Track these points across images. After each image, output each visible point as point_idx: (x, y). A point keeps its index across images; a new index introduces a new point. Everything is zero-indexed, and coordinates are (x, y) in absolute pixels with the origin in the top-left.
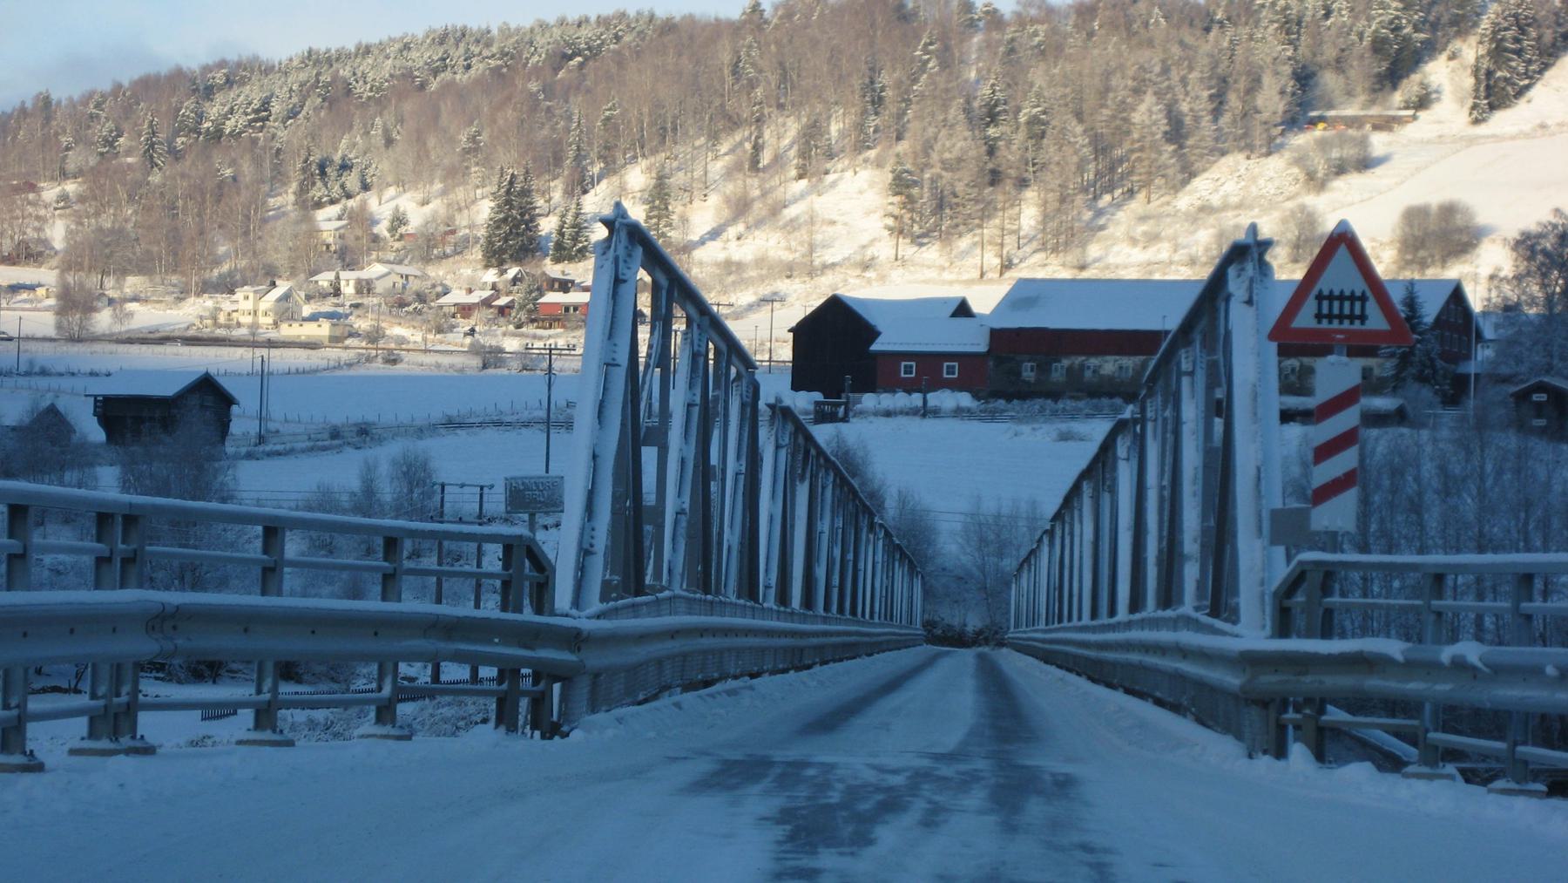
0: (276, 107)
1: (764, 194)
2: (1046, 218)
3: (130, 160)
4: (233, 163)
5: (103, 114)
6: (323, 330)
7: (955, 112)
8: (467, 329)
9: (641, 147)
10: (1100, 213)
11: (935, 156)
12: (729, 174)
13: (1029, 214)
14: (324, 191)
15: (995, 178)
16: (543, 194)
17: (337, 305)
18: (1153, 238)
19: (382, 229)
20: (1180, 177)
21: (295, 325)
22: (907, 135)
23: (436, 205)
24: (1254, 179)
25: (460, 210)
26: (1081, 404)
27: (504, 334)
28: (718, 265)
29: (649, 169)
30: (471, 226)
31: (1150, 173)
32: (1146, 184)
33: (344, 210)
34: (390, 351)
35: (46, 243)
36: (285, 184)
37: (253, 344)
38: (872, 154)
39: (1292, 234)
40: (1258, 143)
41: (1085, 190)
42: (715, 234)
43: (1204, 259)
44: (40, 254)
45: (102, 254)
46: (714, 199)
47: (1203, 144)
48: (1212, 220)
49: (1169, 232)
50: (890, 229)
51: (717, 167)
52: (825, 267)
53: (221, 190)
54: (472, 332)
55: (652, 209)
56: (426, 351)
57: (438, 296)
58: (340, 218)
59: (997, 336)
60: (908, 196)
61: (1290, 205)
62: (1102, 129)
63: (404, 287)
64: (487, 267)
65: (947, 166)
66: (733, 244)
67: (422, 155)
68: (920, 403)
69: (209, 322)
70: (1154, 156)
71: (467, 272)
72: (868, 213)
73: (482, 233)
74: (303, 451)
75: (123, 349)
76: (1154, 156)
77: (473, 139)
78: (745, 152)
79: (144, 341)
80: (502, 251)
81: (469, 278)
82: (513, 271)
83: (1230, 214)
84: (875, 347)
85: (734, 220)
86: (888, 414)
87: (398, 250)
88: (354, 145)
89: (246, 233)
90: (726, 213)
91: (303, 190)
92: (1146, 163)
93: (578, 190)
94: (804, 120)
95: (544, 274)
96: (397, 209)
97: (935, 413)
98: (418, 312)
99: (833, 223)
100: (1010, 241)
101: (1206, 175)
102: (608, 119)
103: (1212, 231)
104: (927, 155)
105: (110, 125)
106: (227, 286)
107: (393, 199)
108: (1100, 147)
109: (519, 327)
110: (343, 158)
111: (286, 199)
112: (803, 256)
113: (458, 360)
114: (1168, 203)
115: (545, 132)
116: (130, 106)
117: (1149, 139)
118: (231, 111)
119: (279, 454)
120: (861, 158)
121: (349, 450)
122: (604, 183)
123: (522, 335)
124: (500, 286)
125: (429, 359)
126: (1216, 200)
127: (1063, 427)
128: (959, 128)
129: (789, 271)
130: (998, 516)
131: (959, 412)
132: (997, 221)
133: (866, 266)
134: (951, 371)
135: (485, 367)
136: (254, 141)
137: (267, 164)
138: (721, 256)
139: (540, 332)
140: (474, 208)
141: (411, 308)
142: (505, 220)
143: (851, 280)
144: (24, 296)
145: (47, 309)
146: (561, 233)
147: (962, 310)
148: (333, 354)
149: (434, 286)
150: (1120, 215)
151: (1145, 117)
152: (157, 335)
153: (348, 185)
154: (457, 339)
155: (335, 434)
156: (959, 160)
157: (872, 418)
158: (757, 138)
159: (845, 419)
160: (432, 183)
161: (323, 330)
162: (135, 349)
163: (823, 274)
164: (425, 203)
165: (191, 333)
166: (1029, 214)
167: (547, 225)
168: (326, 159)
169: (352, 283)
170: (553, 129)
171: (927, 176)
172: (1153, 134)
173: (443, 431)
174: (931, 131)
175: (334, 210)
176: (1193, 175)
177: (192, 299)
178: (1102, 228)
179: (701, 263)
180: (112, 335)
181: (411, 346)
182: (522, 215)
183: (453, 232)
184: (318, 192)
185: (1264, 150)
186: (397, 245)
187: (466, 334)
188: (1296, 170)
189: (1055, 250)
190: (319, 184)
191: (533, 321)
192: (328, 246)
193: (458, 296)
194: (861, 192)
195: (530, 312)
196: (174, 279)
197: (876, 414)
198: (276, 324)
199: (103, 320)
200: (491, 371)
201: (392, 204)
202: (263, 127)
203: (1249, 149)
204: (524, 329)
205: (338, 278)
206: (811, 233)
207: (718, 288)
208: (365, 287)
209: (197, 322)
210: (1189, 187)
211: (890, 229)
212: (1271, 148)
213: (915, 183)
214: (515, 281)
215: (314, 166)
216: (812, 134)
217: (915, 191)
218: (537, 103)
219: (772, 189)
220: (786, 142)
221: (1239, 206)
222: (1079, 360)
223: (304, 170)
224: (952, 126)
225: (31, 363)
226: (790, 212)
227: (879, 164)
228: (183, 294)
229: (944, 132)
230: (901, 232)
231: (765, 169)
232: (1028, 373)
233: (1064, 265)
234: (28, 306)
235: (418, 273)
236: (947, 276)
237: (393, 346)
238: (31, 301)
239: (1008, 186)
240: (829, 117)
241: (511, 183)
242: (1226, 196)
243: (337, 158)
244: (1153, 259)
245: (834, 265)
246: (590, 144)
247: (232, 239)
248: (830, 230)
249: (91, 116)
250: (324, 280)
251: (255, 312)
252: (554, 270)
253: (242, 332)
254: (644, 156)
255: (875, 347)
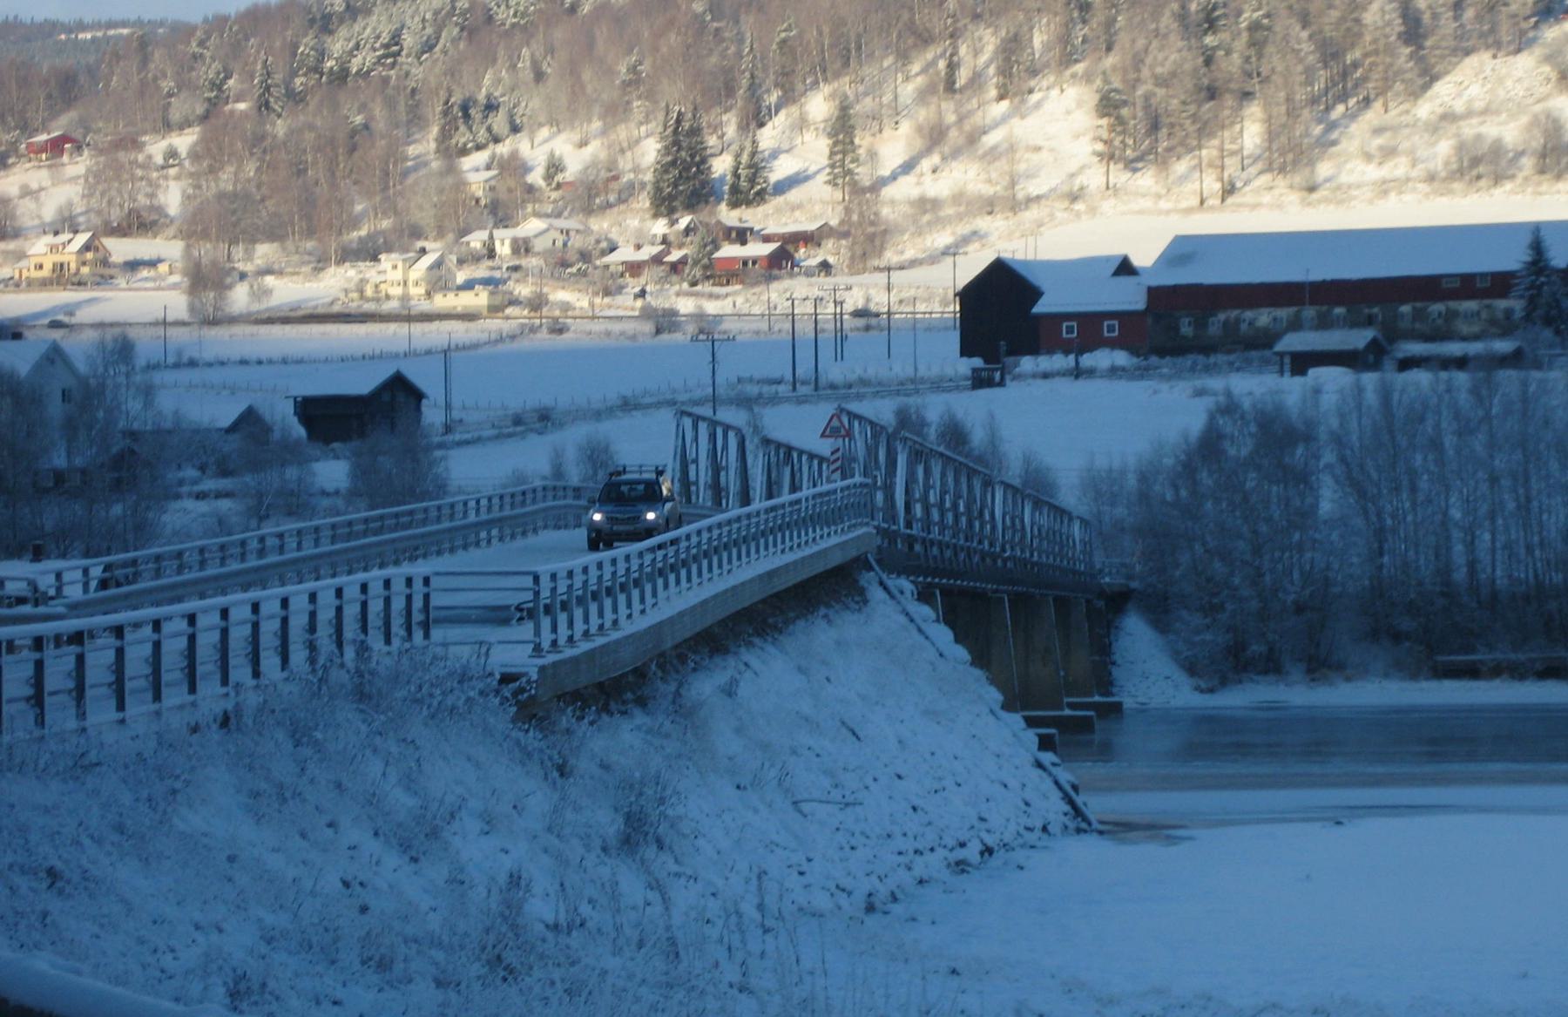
0: (408, 40)
1: (961, 120)
2: (1271, 136)
3: (242, 106)
4: (363, 108)
5: (207, 54)
6: (478, 299)
7: (1167, 21)
8: (637, 290)
9: (822, 73)
10: (1332, 126)
11: (1145, 73)
12: (923, 96)
13: (1251, 132)
14: (468, 136)
15: (1212, 93)
16: (715, 131)
17: (493, 268)
18: (1389, 153)
19: (536, 177)
20: (1420, 82)
21: (451, 295)
22: (1117, 48)
23: (595, 148)
24: (1501, 81)
25: (622, 151)
26: (1232, 357)
27: (678, 294)
28: (912, 203)
29: (832, 96)
30: (636, 169)
31: (1386, 79)
32: (1382, 93)
33: (493, 157)
34: (556, 320)
35: (160, 210)
36: (422, 128)
37: (409, 318)
38: (1079, 68)
39: (1537, 142)
40: (1506, 39)
41: (1314, 101)
42: (908, 167)
43: (1443, 174)
44: (154, 223)
45: (224, 222)
46: (906, 127)
47: (1444, 44)
48: (1453, 129)
49: (1405, 145)
50: (1100, 155)
51: (908, 91)
52: (1031, 201)
53: (356, 139)
54: (642, 294)
55: (835, 144)
56: (593, 318)
57: (604, 253)
58: (488, 168)
59: (1155, 293)
60: (1118, 118)
61: (1538, 108)
62: (1328, 32)
63: (565, 245)
64: (656, 216)
65: (1161, 82)
66: (928, 178)
67: (577, 91)
68: (1073, 364)
69: (355, 295)
70: (1388, 60)
71: (633, 223)
72: (1077, 136)
73: (649, 177)
74: (490, 439)
75: (264, 330)
76: (1388, 60)
77: (633, 69)
78: (938, 73)
79: (286, 321)
80: (671, 197)
81: (637, 230)
82: (684, 221)
83: (1474, 121)
84: (1038, 309)
85: (927, 151)
86: (1046, 376)
87: (555, 201)
88: (499, 80)
89: (386, 188)
90: (919, 144)
91: (445, 136)
92: (1380, 68)
93: (753, 125)
94: (1003, 33)
95: (719, 223)
96: (552, 155)
97: (1091, 373)
98: (582, 274)
99: (1038, 149)
100: (1232, 165)
101: (1448, 78)
102: (784, 41)
103: (1452, 142)
104: (1139, 71)
105: (216, 65)
106: (370, 252)
107: (546, 141)
108: (1330, 53)
109: (694, 284)
110: (488, 97)
111: (424, 146)
112: (1006, 189)
113: (629, 327)
114: (1407, 112)
115: (714, 59)
116: (239, 42)
117: (1382, 41)
118: (357, 47)
119: (467, 443)
120: (1068, 73)
121: (533, 438)
122: (782, 114)
123: (696, 295)
124: (671, 238)
125: (598, 327)
126: (1459, 106)
127: (1198, 383)
128: (1172, 37)
129: (989, 206)
130: (1110, 470)
131: (1114, 372)
132: (1215, 142)
133: (1074, 197)
134: (1110, 329)
135: (658, 331)
136: (385, 81)
137: (402, 107)
138: (915, 193)
139: (717, 290)
140: (638, 150)
141: (574, 270)
142: (673, 163)
143: (1059, 215)
144: (145, 273)
145: (174, 287)
146: (736, 175)
147: (1125, 268)
148: (494, 325)
149: (598, 242)
150: (1354, 127)
151: (1377, 18)
152: (300, 313)
153: (495, 128)
154: (626, 303)
155: (518, 420)
156: (1173, 74)
157: (1030, 381)
158: (952, 55)
159: (1001, 384)
160: (590, 121)
161: (478, 299)
162: (277, 330)
163: (1027, 208)
164: (583, 144)
165: (336, 308)
166: (1251, 132)
167: (721, 166)
168: (469, 99)
169: (507, 242)
170: (723, 56)
171: (1139, 93)
172: (1387, 36)
173: (619, 414)
174: (1141, 43)
175: (480, 158)
176: (1434, 78)
177: (332, 269)
178: (1334, 143)
179: (893, 202)
180: (249, 314)
181: (577, 313)
182: (693, 157)
183: (616, 178)
184: (462, 137)
185: (1512, 48)
186: (554, 195)
187: (637, 296)
188: (1547, 69)
189: (1282, 170)
190: (462, 128)
191: (708, 278)
192: (477, 201)
193: (626, 253)
194: (1068, 113)
195: (705, 268)
196: (310, 245)
197: (1034, 376)
198: (429, 294)
199: (240, 297)
200: (665, 337)
201: (546, 148)
202: (393, 65)
203: (1496, 46)
204: (699, 288)
205: (491, 237)
206: (1012, 162)
207: (912, 229)
208: (522, 247)
209: (342, 296)
210: (1429, 93)
211: (1100, 155)
212: (1521, 45)
213: (1125, 103)
214: (688, 231)
215: (456, 109)
216: (1012, 48)
217: (1125, 112)
218: (702, 27)
219: (970, 113)
220: (983, 58)
221: (1486, 112)
222: (1234, 313)
223: (445, 113)
224: (1165, 36)
225: (179, 353)
226: (991, 139)
227: (1088, 78)
228: (321, 263)
229: (1155, 43)
230: (1111, 157)
231: (961, 90)
232: (1186, 329)
233: (1291, 187)
234: (150, 285)
235: (581, 227)
236: (1164, 205)
237: (557, 313)
238: (154, 279)
239: (1229, 101)
240: (1031, 29)
241: (678, 121)
242: (1470, 101)
243: (481, 97)
244: (1389, 176)
245: (1038, 198)
246: (765, 70)
247: (369, 194)
248: (1035, 157)
249: (195, 57)
250: (476, 240)
251: (405, 283)
252: (729, 216)
253: (392, 306)
254: (826, 80)
255: (1038, 309)
